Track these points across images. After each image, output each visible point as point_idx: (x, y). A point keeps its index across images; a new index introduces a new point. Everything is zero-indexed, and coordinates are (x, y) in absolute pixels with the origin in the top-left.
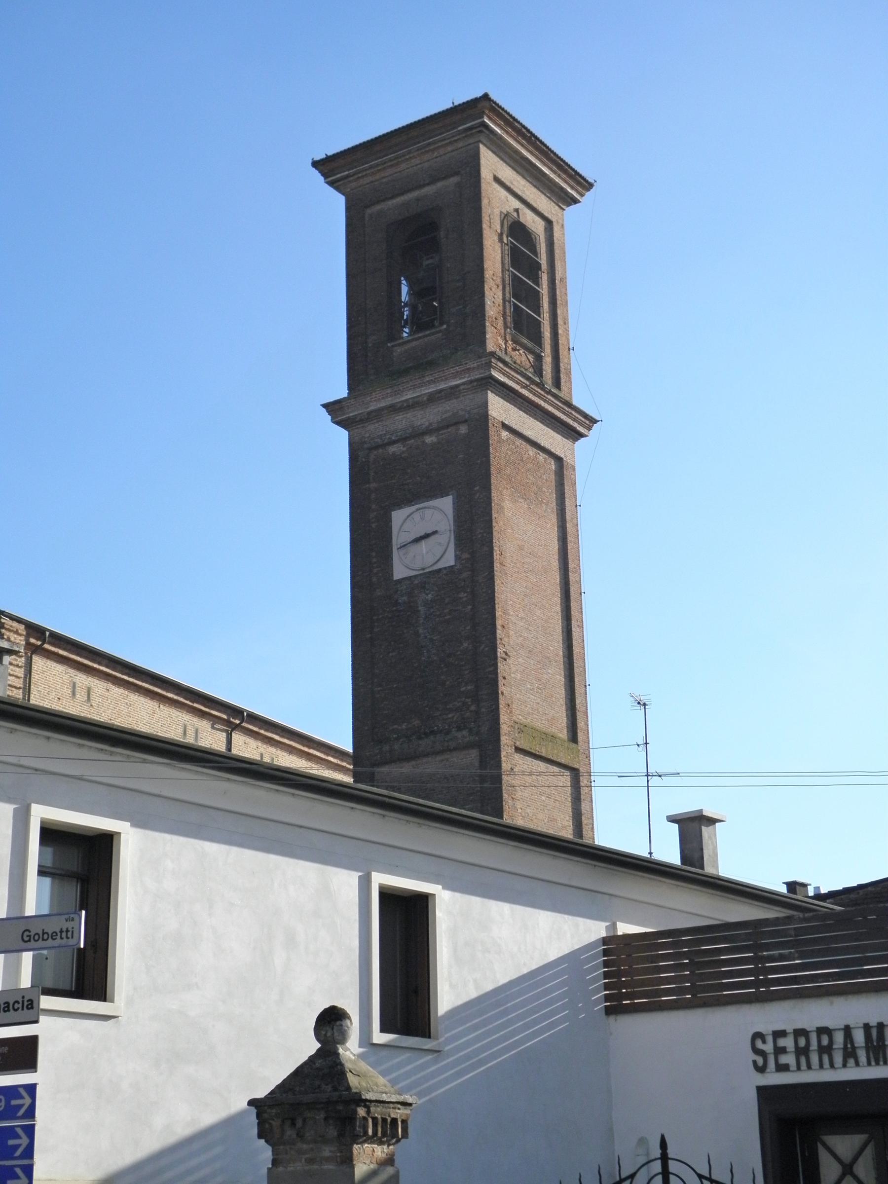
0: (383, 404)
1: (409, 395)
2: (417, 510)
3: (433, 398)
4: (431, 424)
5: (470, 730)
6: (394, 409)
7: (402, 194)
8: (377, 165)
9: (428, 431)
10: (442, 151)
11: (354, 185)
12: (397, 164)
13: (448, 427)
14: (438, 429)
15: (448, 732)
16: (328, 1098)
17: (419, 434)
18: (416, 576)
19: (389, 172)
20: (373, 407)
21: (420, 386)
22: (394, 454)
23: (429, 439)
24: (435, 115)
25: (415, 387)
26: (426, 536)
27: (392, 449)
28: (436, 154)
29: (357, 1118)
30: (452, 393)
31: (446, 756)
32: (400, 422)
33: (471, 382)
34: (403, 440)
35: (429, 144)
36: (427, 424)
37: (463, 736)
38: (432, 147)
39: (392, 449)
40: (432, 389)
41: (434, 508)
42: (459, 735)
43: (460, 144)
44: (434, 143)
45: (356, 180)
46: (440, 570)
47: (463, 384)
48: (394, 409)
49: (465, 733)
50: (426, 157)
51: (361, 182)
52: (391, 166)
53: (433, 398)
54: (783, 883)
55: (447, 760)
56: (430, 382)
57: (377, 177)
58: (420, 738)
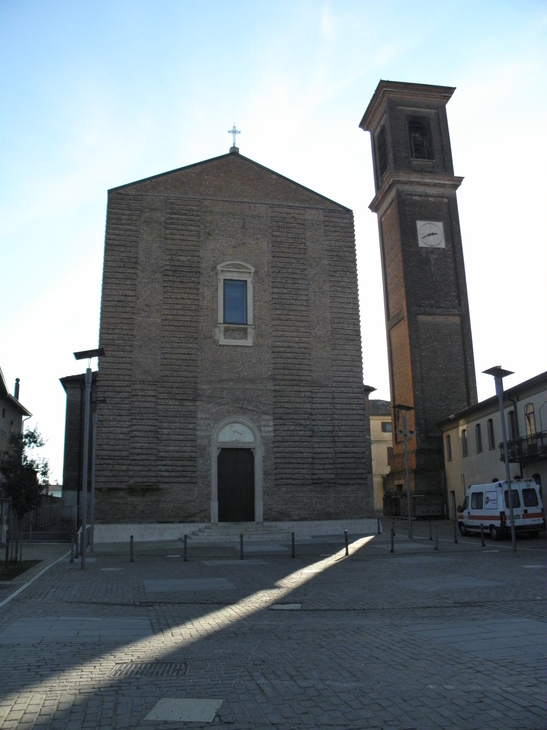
0: (416, 180)
1: (427, 180)
2: (428, 223)
3: (435, 185)
4: (433, 194)
5: (458, 309)
6: (419, 183)
7: (413, 107)
8: (406, 92)
9: (432, 196)
10: (431, 99)
11: (392, 95)
12: (414, 96)
13: (439, 197)
14: (435, 197)
15: (449, 308)
16: (15, 515)
17: (427, 195)
18: (429, 248)
19: (408, 97)
20: (412, 179)
21: (433, 179)
22: (415, 200)
23: (431, 199)
24: (398, 82)
25: (431, 179)
26: (433, 234)
27: (415, 198)
28: (428, 99)
29: (532, 444)
30: (443, 186)
31: (446, 317)
32: (420, 189)
33: (452, 184)
34: (420, 196)
35: (428, 95)
36: (432, 193)
37: (455, 311)
38: (429, 96)
39: (415, 198)
40: (437, 182)
41: (435, 225)
42: (453, 310)
43: (438, 100)
44: (430, 95)
45: (394, 94)
46: (439, 248)
47: (449, 184)
48: (419, 183)
49: (456, 310)
50: (424, 98)
51: (396, 95)
52: (410, 95)
53: (435, 185)
54: (376, 389)
55: (447, 318)
56: (437, 179)
57: (403, 97)
58: (437, 308)
